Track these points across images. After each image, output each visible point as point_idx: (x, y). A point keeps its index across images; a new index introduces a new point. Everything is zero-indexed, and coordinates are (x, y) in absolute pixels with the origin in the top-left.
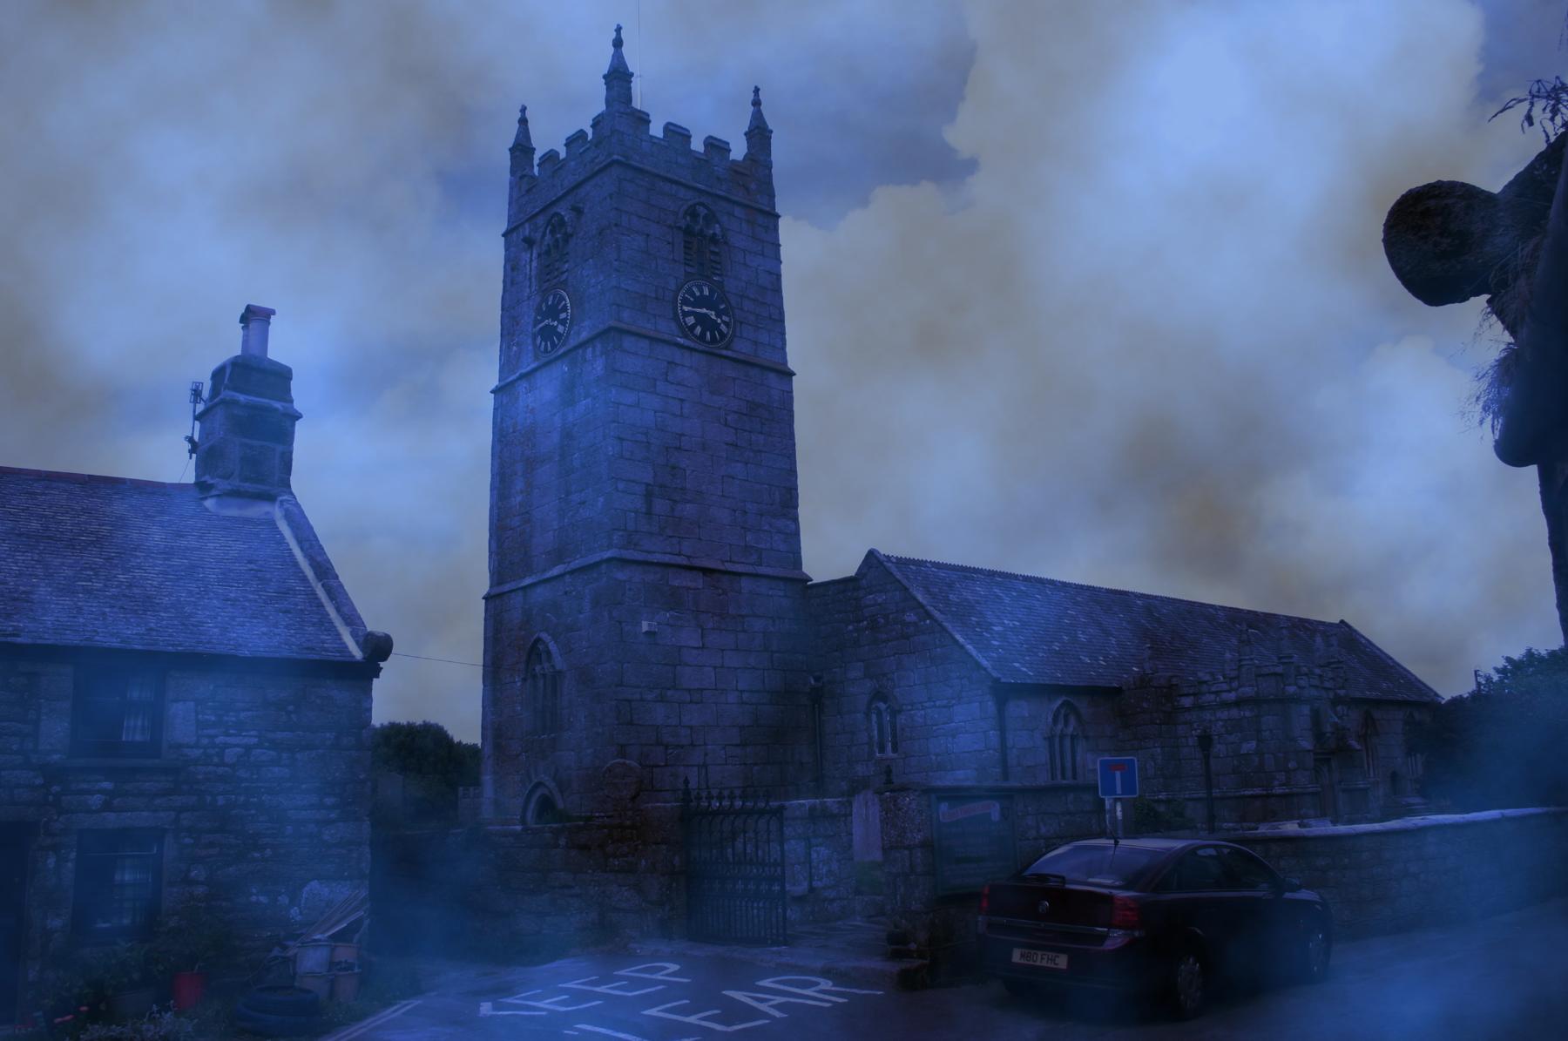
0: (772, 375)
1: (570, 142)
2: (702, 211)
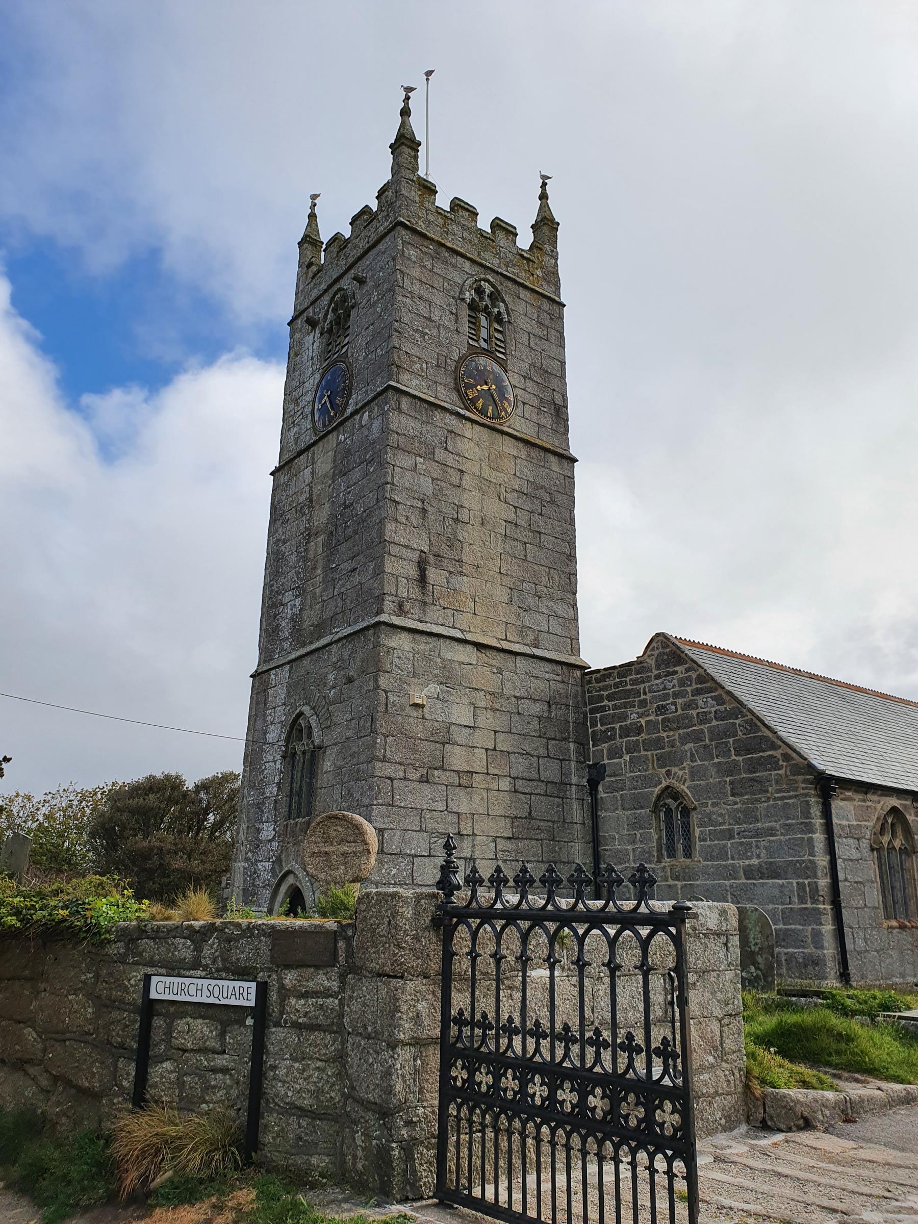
0: (552, 458)
2: (488, 289)
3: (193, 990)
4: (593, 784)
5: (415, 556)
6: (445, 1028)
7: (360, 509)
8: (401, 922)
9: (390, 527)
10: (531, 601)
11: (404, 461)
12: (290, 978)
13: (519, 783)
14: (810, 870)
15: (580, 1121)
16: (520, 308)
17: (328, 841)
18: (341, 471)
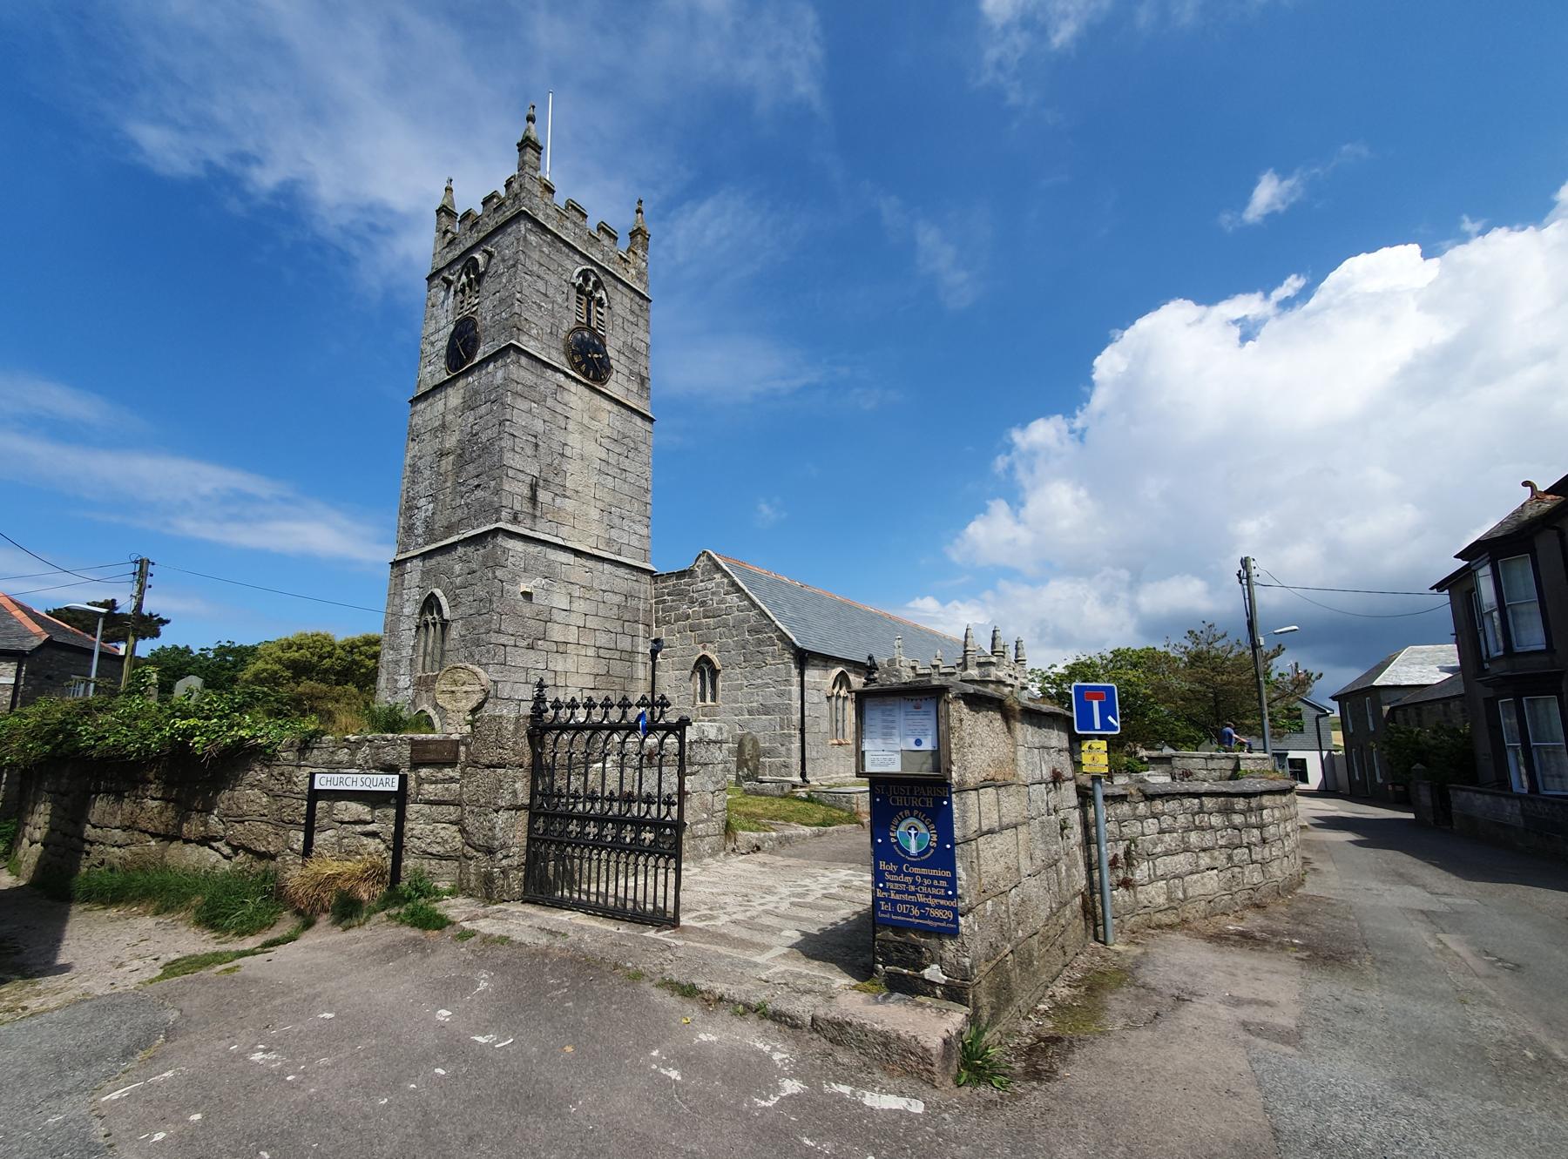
1: (486, 202)
3: (349, 782)
4: (654, 653)
5: (528, 479)
6: (532, 798)
7: (484, 438)
8: (505, 732)
9: (508, 455)
10: (617, 521)
11: (522, 404)
12: (424, 772)
13: (602, 652)
14: (788, 708)
15: (617, 846)
16: (617, 297)
17: (455, 683)
18: (469, 405)
